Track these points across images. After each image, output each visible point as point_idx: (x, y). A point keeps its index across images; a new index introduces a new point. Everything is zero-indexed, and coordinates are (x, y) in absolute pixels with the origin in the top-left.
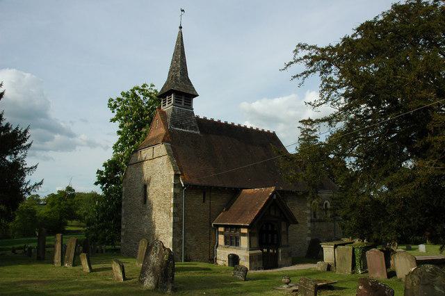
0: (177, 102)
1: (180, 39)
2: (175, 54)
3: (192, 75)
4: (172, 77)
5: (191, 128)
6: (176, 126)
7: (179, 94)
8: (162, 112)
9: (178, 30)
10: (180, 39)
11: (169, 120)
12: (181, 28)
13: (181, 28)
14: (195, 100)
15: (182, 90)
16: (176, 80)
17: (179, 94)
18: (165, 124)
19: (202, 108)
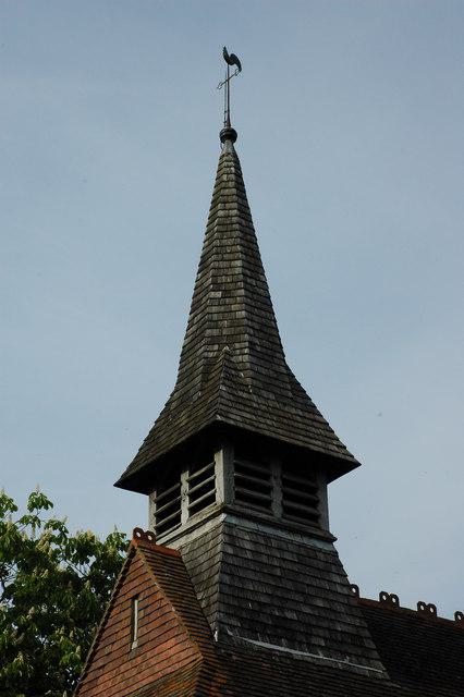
0: (246, 492)
1: (231, 194)
2: (220, 185)
3: (306, 358)
4: (201, 362)
5: (336, 645)
6: (253, 627)
7: (251, 451)
8: (457, 614)
9: (217, 149)
10: (231, 194)
11: (208, 596)
12: (229, 135)
13: (229, 135)
14: (339, 493)
15: (268, 427)
16: (232, 379)
17: (251, 451)
18: (194, 617)
19: (72, 534)
